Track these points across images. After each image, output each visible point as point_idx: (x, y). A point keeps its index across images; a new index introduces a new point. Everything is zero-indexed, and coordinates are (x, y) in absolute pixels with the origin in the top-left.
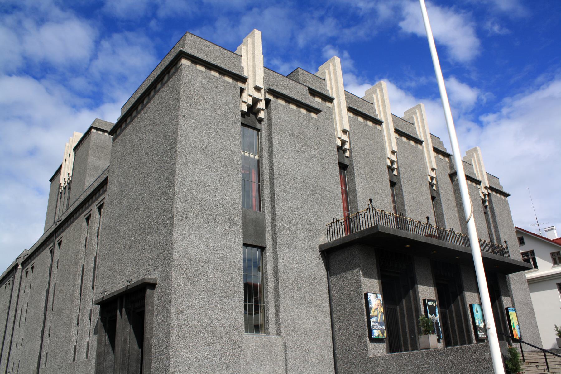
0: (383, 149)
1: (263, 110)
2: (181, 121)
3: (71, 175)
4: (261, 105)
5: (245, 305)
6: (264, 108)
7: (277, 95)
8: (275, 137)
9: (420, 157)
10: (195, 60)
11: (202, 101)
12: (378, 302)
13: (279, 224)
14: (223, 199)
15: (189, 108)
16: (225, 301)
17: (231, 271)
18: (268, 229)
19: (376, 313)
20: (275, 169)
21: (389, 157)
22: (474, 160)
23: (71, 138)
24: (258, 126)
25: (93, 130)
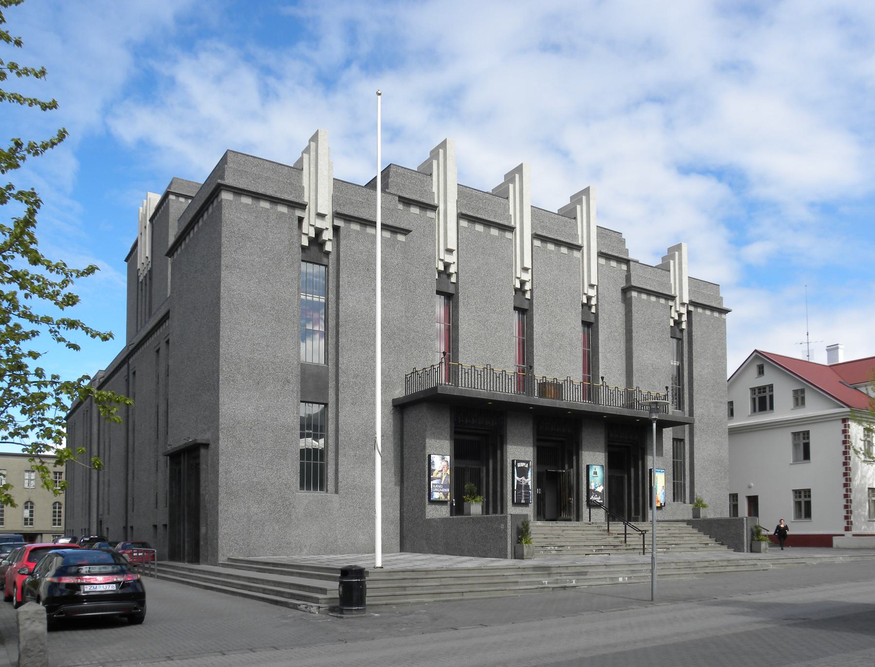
0: (510, 266)
1: (329, 240)
2: (224, 273)
3: (150, 259)
4: (328, 235)
5: (302, 465)
6: (331, 238)
7: (348, 219)
8: (343, 276)
9: (575, 270)
10: (238, 192)
11: (249, 244)
12: (444, 463)
13: (342, 379)
14: (275, 356)
15: (233, 256)
17: (284, 432)
18: (332, 384)
19: (439, 475)
20: (341, 315)
21: (518, 276)
22: (674, 263)
23: (145, 201)
24: (325, 261)
25: (172, 197)
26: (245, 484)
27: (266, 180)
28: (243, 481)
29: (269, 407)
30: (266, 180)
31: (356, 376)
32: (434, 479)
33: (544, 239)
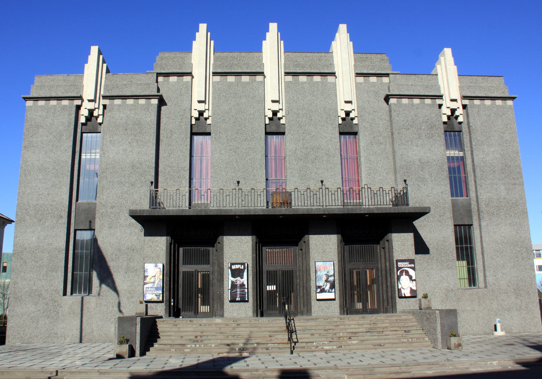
0: (263, 101)
16: (50, 273)
17: (56, 253)
19: (152, 280)
26: (27, 291)
27: (57, 87)
28: (26, 289)
29: (47, 236)
30: (57, 87)
31: (112, 207)
32: (147, 283)
33: (295, 74)
